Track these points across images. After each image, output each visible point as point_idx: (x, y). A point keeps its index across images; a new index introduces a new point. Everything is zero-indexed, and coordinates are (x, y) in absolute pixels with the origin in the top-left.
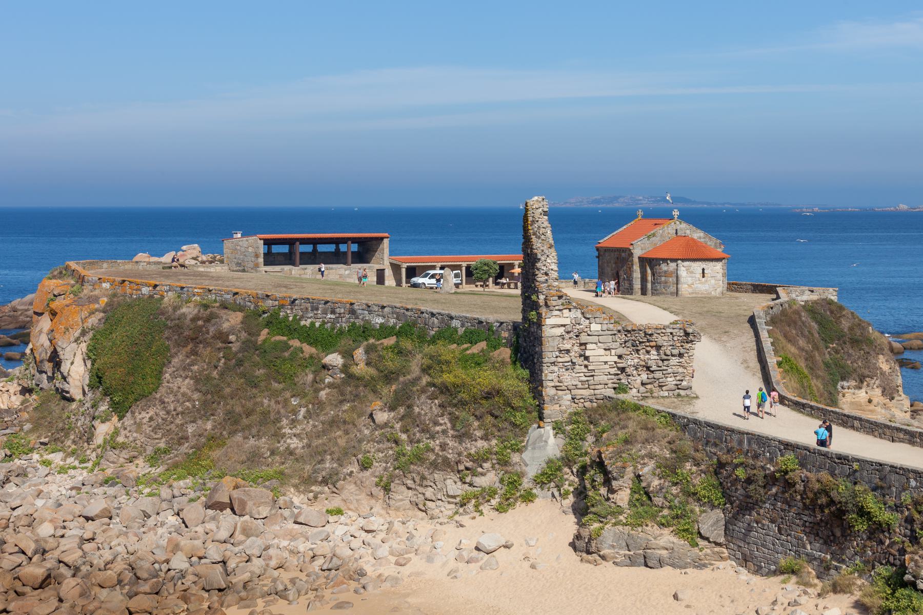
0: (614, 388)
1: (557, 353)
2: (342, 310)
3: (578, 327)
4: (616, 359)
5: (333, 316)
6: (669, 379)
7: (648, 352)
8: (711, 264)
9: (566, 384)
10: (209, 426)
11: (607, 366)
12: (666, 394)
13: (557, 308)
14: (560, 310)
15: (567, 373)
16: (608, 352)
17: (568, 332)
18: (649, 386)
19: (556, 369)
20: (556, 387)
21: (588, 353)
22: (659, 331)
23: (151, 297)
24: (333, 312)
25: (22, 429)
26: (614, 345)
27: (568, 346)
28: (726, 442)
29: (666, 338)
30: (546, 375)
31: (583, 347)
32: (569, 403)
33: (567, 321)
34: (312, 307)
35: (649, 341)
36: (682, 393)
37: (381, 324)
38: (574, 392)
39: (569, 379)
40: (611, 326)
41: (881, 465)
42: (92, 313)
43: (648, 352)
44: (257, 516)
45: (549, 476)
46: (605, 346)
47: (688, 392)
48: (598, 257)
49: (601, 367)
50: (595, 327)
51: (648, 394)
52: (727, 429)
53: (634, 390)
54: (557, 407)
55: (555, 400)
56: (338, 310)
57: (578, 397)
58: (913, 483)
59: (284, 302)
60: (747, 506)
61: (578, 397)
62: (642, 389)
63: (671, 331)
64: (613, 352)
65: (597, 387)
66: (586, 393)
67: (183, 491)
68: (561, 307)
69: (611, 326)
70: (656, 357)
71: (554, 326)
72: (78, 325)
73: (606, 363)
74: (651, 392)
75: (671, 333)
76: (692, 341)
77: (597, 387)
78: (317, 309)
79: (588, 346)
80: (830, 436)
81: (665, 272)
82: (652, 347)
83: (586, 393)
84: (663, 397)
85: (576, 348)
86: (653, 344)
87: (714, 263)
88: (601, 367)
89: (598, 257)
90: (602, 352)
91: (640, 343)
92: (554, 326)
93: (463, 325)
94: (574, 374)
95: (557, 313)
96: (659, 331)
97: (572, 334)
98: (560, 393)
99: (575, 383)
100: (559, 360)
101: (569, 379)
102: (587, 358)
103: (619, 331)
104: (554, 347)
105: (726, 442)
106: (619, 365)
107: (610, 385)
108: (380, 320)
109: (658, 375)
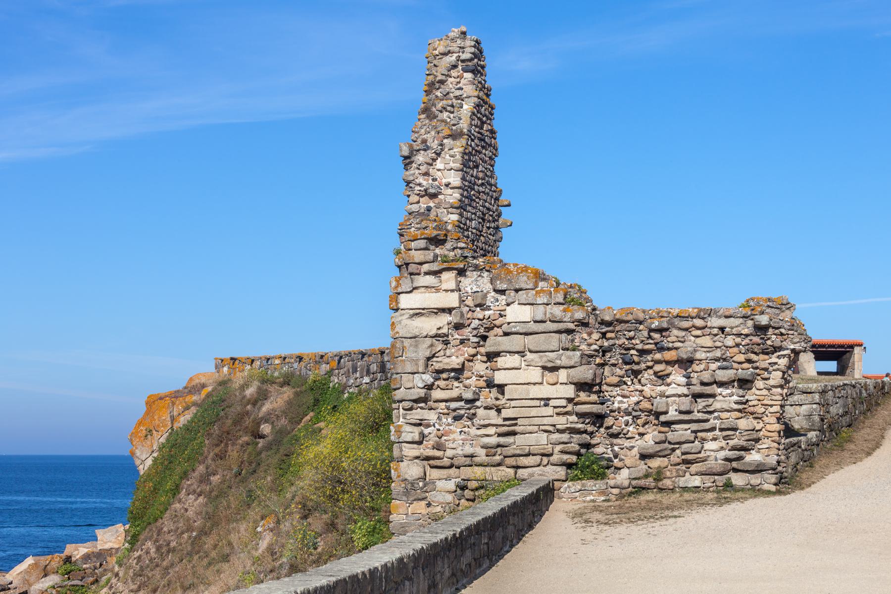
0: (569, 466)
3: (479, 313)
4: (570, 391)
6: (710, 445)
7: (662, 377)
9: (449, 453)
11: (549, 411)
12: (696, 481)
13: (426, 268)
14: (436, 273)
15: (456, 428)
16: (550, 377)
17: (458, 327)
18: (656, 463)
19: (432, 416)
20: (428, 458)
22: (685, 324)
26: (565, 359)
29: (707, 341)
30: (399, 432)
32: (449, 498)
33: (452, 300)
35: (661, 349)
38: (466, 472)
39: (460, 440)
40: (557, 311)
42: (187, 408)
43: (662, 377)
49: (534, 412)
50: (518, 313)
51: (649, 482)
54: (420, 507)
55: (418, 490)
62: (642, 467)
63: (722, 322)
68: (435, 267)
69: (557, 311)
70: (685, 390)
71: (418, 313)
72: (166, 425)
73: (546, 401)
74: (659, 475)
75: (722, 329)
80: (360, 551)
84: (685, 489)
86: (670, 355)
88: (534, 412)
90: (535, 374)
91: (642, 352)
92: (418, 313)
94: (473, 431)
95: (430, 280)
96: (685, 324)
97: (467, 332)
99: (469, 450)
101: (460, 440)
103: (584, 324)
104: (415, 362)
107: (555, 458)
109: (682, 432)
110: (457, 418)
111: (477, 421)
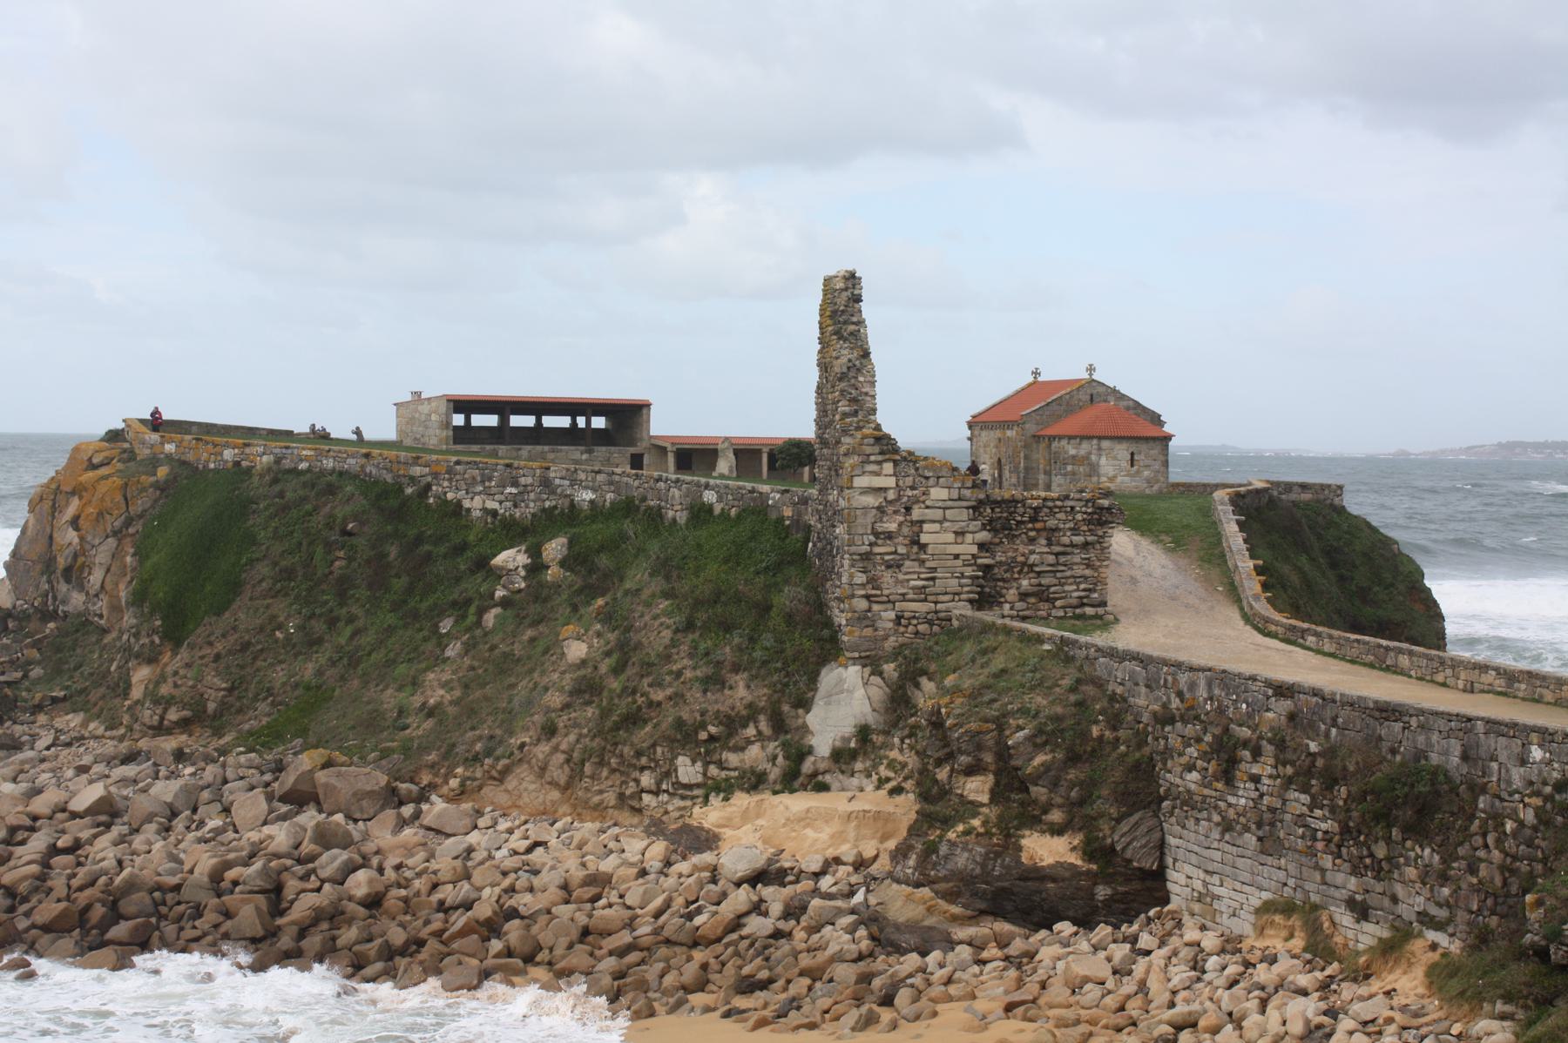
1: (872, 538)
2: (529, 480)
5: (514, 490)
8: (1144, 447)
9: (886, 592)
10: (310, 668)
11: (959, 563)
21: (924, 539)
22: (1050, 504)
23: (237, 464)
24: (515, 484)
25: (25, 676)
27: (893, 527)
28: (1165, 685)
31: (916, 529)
32: (891, 625)
34: (482, 475)
36: (1089, 611)
37: (592, 502)
41: (1469, 720)
44: (357, 816)
45: (856, 751)
46: (956, 527)
47: (1100, 611)
48: (970, 439)
49: (949, 563)
52: (1165, 662)
53: (1007, 606)
56: (523, 480)
57: (907, 614)
58: (1537, 753)
59: (438, 469)
60: (1218, 752)
61: (907, 614)
64: (969, 538)
65: (941, 598)
66: (922, 608)
67: (241, 772)
68: (880, 458)
69: (967, 493)
73: (957, 557)
76: (1107, 522)
77: (941, 598)
78: (490, 479)
79: (926, 527)
81: (1073, 457)
82: (1038, 531)
83: (922, 608)
85: (905, 530)
87: (1151, 444)
89: (970, 439)
91: (1019, 523)
93: (720, 500)
94: (901, 577)
98: (876, 607)
100: (877, 550)
102: (923, 547)
105: (1165, 685)
106: (980, 561)
107: (964, 596)
108: (588, 495)
110: (888, 567)
111: (904, 569)
